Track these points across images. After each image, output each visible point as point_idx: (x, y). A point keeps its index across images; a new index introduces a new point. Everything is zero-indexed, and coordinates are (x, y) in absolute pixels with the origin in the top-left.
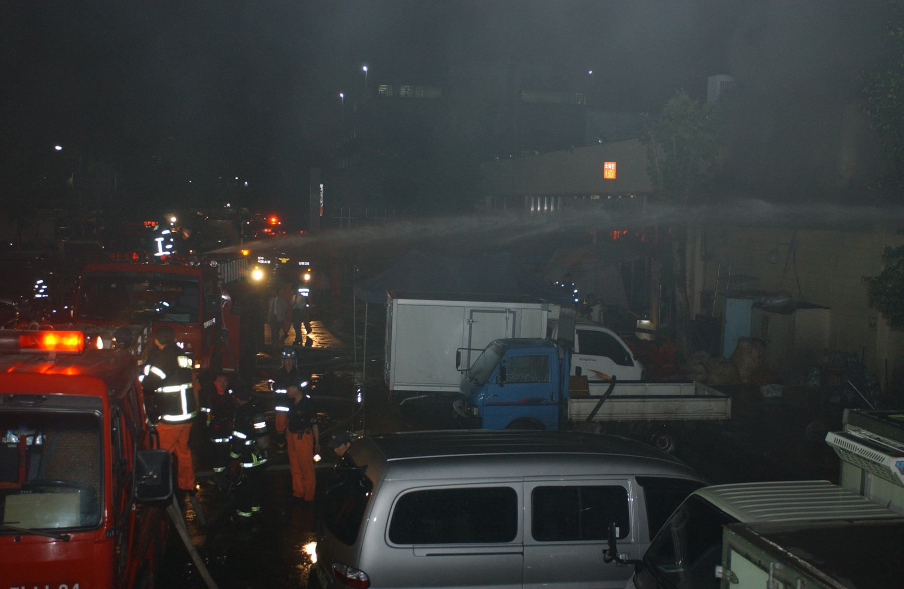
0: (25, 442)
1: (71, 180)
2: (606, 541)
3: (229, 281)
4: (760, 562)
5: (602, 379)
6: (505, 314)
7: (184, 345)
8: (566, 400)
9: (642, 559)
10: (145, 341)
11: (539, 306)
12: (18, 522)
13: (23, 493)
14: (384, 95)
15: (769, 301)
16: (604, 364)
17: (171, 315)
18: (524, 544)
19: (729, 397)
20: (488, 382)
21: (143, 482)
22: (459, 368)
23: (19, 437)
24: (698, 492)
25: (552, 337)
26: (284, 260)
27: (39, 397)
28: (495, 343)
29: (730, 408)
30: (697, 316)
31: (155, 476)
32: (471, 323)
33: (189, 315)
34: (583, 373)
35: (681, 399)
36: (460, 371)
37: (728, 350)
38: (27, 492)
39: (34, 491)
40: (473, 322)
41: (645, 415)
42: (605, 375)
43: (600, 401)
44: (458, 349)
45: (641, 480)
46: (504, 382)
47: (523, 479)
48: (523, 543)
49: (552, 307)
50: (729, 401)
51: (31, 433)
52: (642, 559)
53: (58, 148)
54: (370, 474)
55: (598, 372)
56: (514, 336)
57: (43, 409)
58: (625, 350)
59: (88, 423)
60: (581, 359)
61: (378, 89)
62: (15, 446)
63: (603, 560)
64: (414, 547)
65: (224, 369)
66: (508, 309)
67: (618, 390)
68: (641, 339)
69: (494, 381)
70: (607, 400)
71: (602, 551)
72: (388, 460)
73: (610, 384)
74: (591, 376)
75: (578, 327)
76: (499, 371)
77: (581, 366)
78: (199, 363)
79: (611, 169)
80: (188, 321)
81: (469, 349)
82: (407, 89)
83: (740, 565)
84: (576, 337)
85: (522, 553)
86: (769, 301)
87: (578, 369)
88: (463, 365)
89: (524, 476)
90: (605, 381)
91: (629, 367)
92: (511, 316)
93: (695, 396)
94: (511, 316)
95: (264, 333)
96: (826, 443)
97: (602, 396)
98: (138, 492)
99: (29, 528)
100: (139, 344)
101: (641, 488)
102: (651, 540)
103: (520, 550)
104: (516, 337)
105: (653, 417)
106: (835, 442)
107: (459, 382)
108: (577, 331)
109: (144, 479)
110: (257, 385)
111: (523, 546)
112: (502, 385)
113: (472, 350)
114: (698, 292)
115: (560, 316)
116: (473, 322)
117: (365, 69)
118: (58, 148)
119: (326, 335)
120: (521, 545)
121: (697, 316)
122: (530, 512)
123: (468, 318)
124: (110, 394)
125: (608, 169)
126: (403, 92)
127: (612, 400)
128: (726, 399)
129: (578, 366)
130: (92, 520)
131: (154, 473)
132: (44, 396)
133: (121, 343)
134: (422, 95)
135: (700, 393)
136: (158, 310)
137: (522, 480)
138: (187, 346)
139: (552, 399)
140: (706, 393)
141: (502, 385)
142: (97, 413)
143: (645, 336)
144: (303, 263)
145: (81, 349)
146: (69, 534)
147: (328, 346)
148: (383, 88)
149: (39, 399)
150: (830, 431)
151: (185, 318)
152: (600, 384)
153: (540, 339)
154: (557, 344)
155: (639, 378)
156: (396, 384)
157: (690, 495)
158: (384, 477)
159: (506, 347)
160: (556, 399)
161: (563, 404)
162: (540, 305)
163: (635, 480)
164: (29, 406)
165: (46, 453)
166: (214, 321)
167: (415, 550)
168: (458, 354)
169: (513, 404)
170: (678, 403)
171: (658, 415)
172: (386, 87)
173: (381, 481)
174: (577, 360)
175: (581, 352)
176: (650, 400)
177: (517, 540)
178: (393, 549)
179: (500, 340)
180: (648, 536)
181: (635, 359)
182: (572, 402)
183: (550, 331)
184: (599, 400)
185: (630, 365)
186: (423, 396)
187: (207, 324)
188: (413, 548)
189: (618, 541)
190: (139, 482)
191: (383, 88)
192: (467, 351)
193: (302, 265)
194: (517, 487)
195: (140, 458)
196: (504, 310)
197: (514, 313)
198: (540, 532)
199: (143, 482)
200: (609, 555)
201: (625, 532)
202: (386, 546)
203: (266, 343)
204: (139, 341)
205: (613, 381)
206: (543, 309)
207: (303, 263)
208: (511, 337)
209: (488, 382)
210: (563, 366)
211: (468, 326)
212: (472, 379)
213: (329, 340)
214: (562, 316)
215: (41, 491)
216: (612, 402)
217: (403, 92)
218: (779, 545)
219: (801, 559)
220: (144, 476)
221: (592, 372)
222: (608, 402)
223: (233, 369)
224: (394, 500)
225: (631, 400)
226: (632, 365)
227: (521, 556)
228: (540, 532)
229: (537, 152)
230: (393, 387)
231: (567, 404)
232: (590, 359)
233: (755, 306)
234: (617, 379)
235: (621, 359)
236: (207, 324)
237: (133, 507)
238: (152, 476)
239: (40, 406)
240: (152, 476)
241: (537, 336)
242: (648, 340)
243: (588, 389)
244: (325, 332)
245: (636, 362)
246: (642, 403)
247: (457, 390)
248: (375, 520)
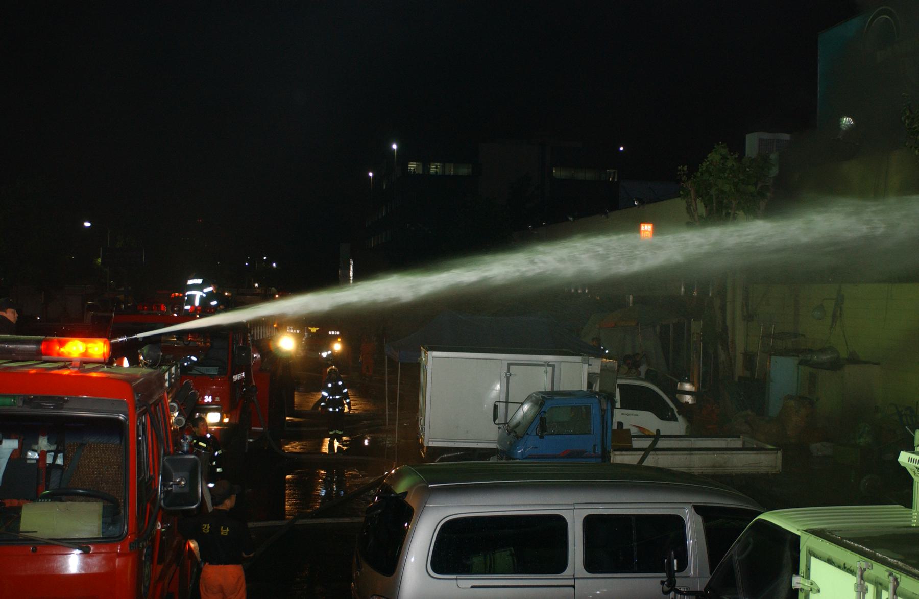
0: (45, 459)
1: (99, 260)
2: (664, 575)
3: (259, 338)
4: (845, 564)
5: (643, 434)
6: (544, 367)
7: (212, 399)
8: (609, 453)
9: (703, 590)
10: (173, 381)
11: (578, 359)
12: (473, 587)
13: (41, 501)
14: (413, 172)
15: (816, 357)
16: (647, 420)
17: (199, 367)
18: (575, 577)
19: (780, 450)
20: (528, 434)
21: (170, 489)
22: (497, 422)
23: (39, 453)
24: (761, 517)
25: (593, 389)
26: (314, 330)
27: (62, 399)
28: (534, 395)
29: (781, 461)
30: (740, 378)
31: (183, 483)
32: (508, 376)
33: (217, 368)
34: (625, 428)
35: (729, 452)
36: (498, 426)
37: (774, 407)
38: (43, 500)
39: (53, 500)
40: (510, 375)
41: (692, 469)
42: (648, 431)
43: (645, 453)
44: (496, 402)
45: (698, 509)
46: (545, 433)
47: (573, 506)
48: (574, 576)
49: (592, 360)
50: (780, 454)
51: (53, 447)
52: (703, 590)
53: (87, 224)
54: (411, 500)
55: (642, 428)
56: (553, 388)
57: (65, 412)
58: (668, 405)
59: (113, 427)
60: (622, 414)
61: (408, 167)
62: (34, 461)
63: (661, 592)
64: (458, 577)
65: (253, 428)
66: (547, 362)
67: (661, 444)
68: (681, 401)
69: (534, 433)
70: (651, 453)
71: (660, 582)
72: (430, 486)
73: (653, 439)
74: (634, 431)
75: (619, 382)
76: (539, 422)
77: (623, 422)
78: (227, 417)
79: (648, 231)
80: (217, 374)
81: (507, 402)
82: (436, 166)
83: (818, 568)
84: (618, 391)
85: (574, 586)
86: (816, 357)
87: (620, 424)
88: (501, 418)
89: (574, 504)
90: (649, 436)
91: (673, 423)
92: (550, 369)
93: (744, 449)
94: (550, 369)
95: (294, 399)
96: (898, 463)
97: (646, 449)
98: (164, 499)
99: (47, 538)
100: (166, 381)
101: (699, 518)
102: (711, 574)
103: (571, 582)
104: (555, 390)
105: (700, 471)
106: (909, 461)
107: (496, 438)
108: (618, 384)
109: (171, 486)
110: (286, 446)
111: (575, 578)
112: (542, 437)
113: (510, 403)
114: (741, 353)
115: (602, 370)
116: (510, 375)
117: (394, 146)
118: (87, 224)
119: (356, 402)
120: (573, 577)
121: (740, 378)
122: (582, 537)
123: (506, 372)
124: (137, 398)
125: (645, 231)
126: (433, 169)
127: (657, 453)
128: (776, 452)
129: (619, 421)
130: (113, 530)
131: (182, 480)
132: (66, 399)
133: (148, 360)
134: (452, 172)
135: (748, 445)
136: (186, 364)
137: (573, 508)
138: (215, 399)
139: (595, 452)
140: (755, 446)
141: (542, 437)
142: (121, 417)
143: (688, 399)
144: (333, 333)
145: (107, 357)
146: (90, 546)
147: (359, 411)
148: (412, 166)
149: (60, 402)
150: (903, 451)
151: (213, 371)
152: (644, 439)
153: (581, 391)
154: (599, 395)
155: (683, 433)
156: (430, 440)
157: (754, 520)
158: (426, 503)
159: (543, 401)
160: (599, 451)
161: (605, 456)
162: (580, 358)
163: (693, 510)
164: (50, 410)
165: (67, 468)
166: (243, 375)
167: (459, 581)
168: (496, 407)
169: (554, 457)
170: (726, 456)
171: (705, 468)
172: (416, 165)
173: (422, 507)
174: (620, 415)
175: (622, 407)
176: (696, 452)
177: (568, 572)
178: (435, 580)
179: (539, 392)
180: (708, 570)
181: (679, 414)
182: (615, 455)
183: (590, 385)
184: (643, 453)
185: (674, 421)
186: (459, 453)
187: (236, 378)
188: (457, 579)
189: (676, 574)
190: (166, 489)
191: (412, 166)
192: (509, 401)
193: (332, 335)
194: (567, 515)
195: (167, 463)
196: (542, 363)
197: (553, 366)
198: (592, 564)
199: (170, 489)
200: (668, 586)
201: (683, 565)
202: (432, 579)
203: (295, 408)
204: (167, 376)
205: (658, 436)
206: (583, 362)
207: (333, 333)
208: (550, 390)
209: (528, 434)
210: (606, 417)
211: (506, 379)
212: (509, 433)
213: (360, 406)
214: (604, 369)
215: (61, 501)
216: (657, 454)
217: (433, 169)
218: (864, 546)
219: (892, 558)
220: (171, 483)
221: (636, 428)
222: (653, 455)
223: (262, 429)
224: (438, 524)
225: (677, 453)
226: (676, 420)
227: (572, 589)
228: (592, 564)
229: (571, 219)
230: (428, 443)
231: (610, 457)
232: (632, 415)
233: (801, 363)
234: (661, 434)
235: (663, 413)
236: (236, 378)
237: (159, 526)
238: (180, 482)
239: (62, 408)
240: (180, 482)
241: (576, 388)
242: (690, 403)
243: (631, 443)
244: (355, 399)
245: (680, 418)
246: (688, 456)
247: (493, 446)
248: (412, 560)
